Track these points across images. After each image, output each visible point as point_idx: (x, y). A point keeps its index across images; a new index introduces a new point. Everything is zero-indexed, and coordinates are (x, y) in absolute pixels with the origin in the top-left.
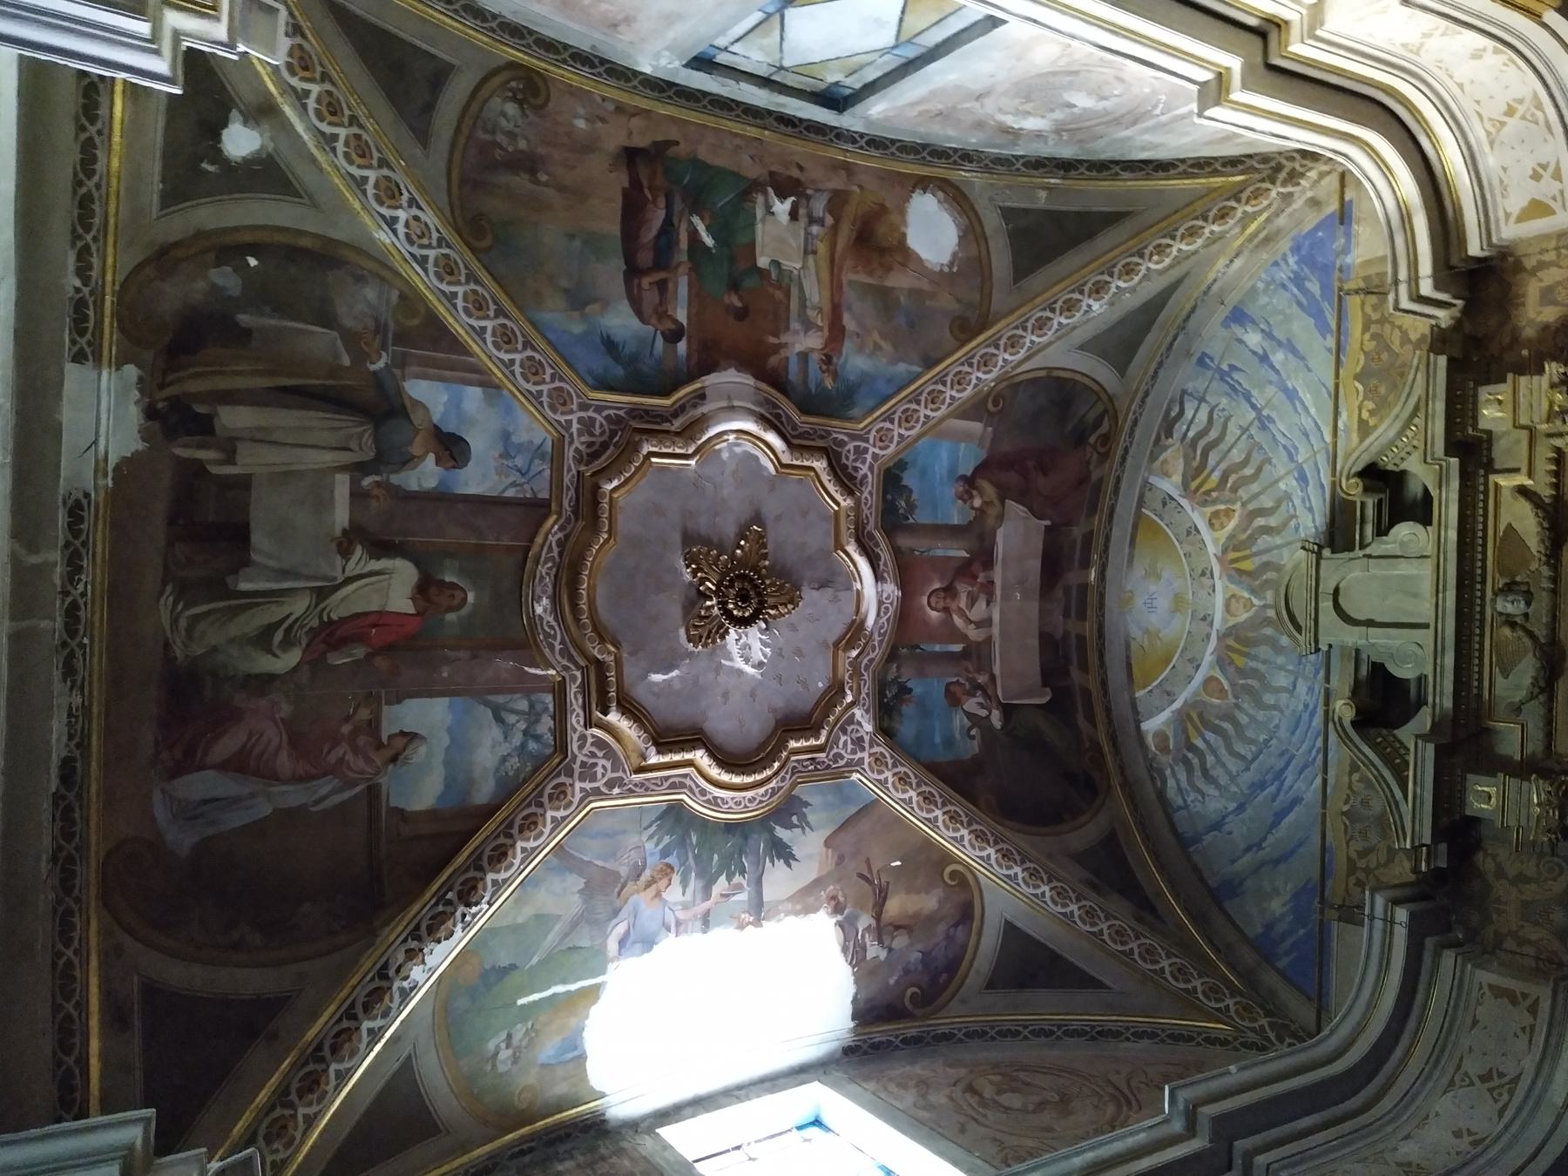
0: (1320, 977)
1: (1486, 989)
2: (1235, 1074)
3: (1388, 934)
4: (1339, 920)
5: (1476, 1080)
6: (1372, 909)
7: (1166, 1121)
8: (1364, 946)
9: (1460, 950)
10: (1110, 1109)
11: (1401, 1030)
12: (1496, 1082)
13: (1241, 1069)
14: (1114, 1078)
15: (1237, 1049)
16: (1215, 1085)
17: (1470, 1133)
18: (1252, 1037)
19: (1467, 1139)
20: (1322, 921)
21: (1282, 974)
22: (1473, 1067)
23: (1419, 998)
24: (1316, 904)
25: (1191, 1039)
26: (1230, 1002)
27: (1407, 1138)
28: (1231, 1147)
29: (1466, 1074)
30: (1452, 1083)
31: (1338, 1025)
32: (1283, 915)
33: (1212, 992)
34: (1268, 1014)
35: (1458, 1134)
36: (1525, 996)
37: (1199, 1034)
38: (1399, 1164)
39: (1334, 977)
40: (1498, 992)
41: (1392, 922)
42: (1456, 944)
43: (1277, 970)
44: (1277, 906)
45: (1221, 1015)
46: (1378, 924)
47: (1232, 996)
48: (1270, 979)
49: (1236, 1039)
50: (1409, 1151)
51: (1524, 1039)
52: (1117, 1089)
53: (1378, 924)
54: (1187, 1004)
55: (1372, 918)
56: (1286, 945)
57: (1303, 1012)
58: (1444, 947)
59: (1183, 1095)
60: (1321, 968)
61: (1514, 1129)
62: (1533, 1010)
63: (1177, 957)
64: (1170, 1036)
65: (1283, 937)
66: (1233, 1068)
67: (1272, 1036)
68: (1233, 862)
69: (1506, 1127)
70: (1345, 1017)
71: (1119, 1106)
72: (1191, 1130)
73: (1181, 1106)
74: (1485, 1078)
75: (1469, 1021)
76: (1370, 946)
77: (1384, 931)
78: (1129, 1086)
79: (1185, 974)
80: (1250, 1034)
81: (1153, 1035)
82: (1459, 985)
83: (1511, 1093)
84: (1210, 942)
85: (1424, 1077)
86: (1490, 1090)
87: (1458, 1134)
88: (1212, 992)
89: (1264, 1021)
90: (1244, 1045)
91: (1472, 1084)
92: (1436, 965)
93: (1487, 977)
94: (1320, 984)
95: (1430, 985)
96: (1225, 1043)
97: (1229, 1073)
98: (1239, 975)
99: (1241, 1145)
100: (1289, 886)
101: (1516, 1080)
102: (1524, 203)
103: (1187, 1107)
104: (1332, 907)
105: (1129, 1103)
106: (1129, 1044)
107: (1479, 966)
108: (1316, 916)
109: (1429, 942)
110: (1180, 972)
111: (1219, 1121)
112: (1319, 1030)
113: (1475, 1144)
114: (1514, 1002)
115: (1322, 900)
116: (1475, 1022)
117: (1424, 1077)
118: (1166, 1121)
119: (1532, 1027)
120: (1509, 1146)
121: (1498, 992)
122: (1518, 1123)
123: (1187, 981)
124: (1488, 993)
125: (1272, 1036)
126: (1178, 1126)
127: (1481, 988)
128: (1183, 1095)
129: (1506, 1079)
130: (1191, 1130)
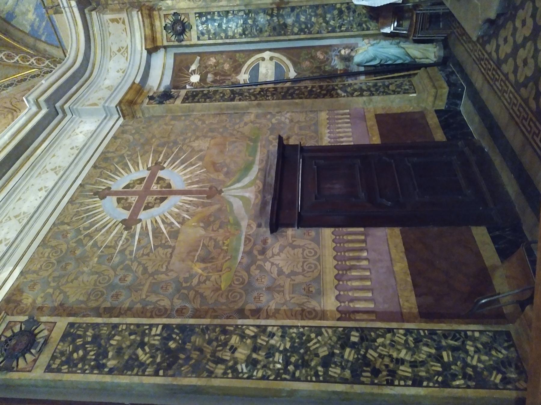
0: (57, 36)
1: (109, 21)
2: (45, 83)
3: (72, 12)
4: (55, 14)
5: (117, 53)
6: (63, 4)
7: (30, 109)
8: (67, 22)
9: (96, 10)
10: (10, 116)
11: (90, 47)
12: (122, 50)
13: (46, 81)
14: (5, 105)
15: (43, 76)
16: (41, 89)
17: (121, 69)
18: (46, 69)
19: (121, 72)
20: (49, 17)
21: (45, 42)
22: (115, 48)
23: (91, 32)
24: (44, 10)
25: (25, 80)
26: (32, 60)
27: (105, 79)
28: (55, 107)
29: (113, 52)
30: (111, 56)
31: (70, 51)
32: (35, 19)
33: (24, 59)
34: (48, 59)
35: (118, 71)
36: (120, 19)
37: (28, 76)
38: (106, 88)
39: (61, 34)
40: (113, 21)
41: (71, 7)
42: (94, 9)
43: (43, 42)
44: (31, 16)
45: (31, 66)
46: (67, 9)
47: (32, 57)
48: (42, 46)
49: (41, 72)
50: (107, 83)
51: (125, 33)
52: (10, 108)
53: (67, 9)
54: (18, 67)
55: (64, 8)
56: (41, 31)
57: (57, 53)
58: (92, 11)
59: (31, 98)
60: (56, 32)
61: (131, 63)
62: (124, 23)
63: (4, 51)
64: (18, 82)
65: (39, 27)
66: (43, 81)
67: (52, 66)
68: (6, 3)
69: (129, 64)
70: (71, 48)
71: (12, 114)
72: (40, 108)
73: (32, 102)
74: (119, 50)
75: (108, 34)
76: (69, 22)
77: (70, 12)
78: (13, 106)
79: (11, 56)
80: (45, 68)
81: (11, 85)
82: (101, 25)
83: (127, 52)
84: (14, 41)
85: (102, 58)
86: (122, 54)
87: (118, 71)
88: (24, 59)
89: (47, 62)
90: (44, 73)
91: (116, 54)
92: (91, 19)
93: (108, 17)
94: (59, 39)
95: (92, 27)
96: (38, 75)
97: (42, 84)
98: (32, 49)
99: (58, 105)
100: (31, 6)
101: (127, 48)
102: (535, 301)
103: (34, 101)
104: (48, 8)
105: (15, 111)
106: (5, 91)
107: (103, 14)
108: (46, 15)
109: (86, 11)
110: (9, 57)
111: (47, 101)
112: (66, 56)
113: (123, 72)
114: (118, 22)
115: (45, 7)
116: (110, 34)
117: (102, 58)
118: (30, 109)
119: (125, 28)
120: (132, 68)
121: (113, 21)
122: (132, 60)
123: (13, 59)
124: (110, 23)
125: (52, 66)
126: (34, 109)
127: (107, 21)
128: (31, 98)
129: (124, 49)
130: (40, 108)
